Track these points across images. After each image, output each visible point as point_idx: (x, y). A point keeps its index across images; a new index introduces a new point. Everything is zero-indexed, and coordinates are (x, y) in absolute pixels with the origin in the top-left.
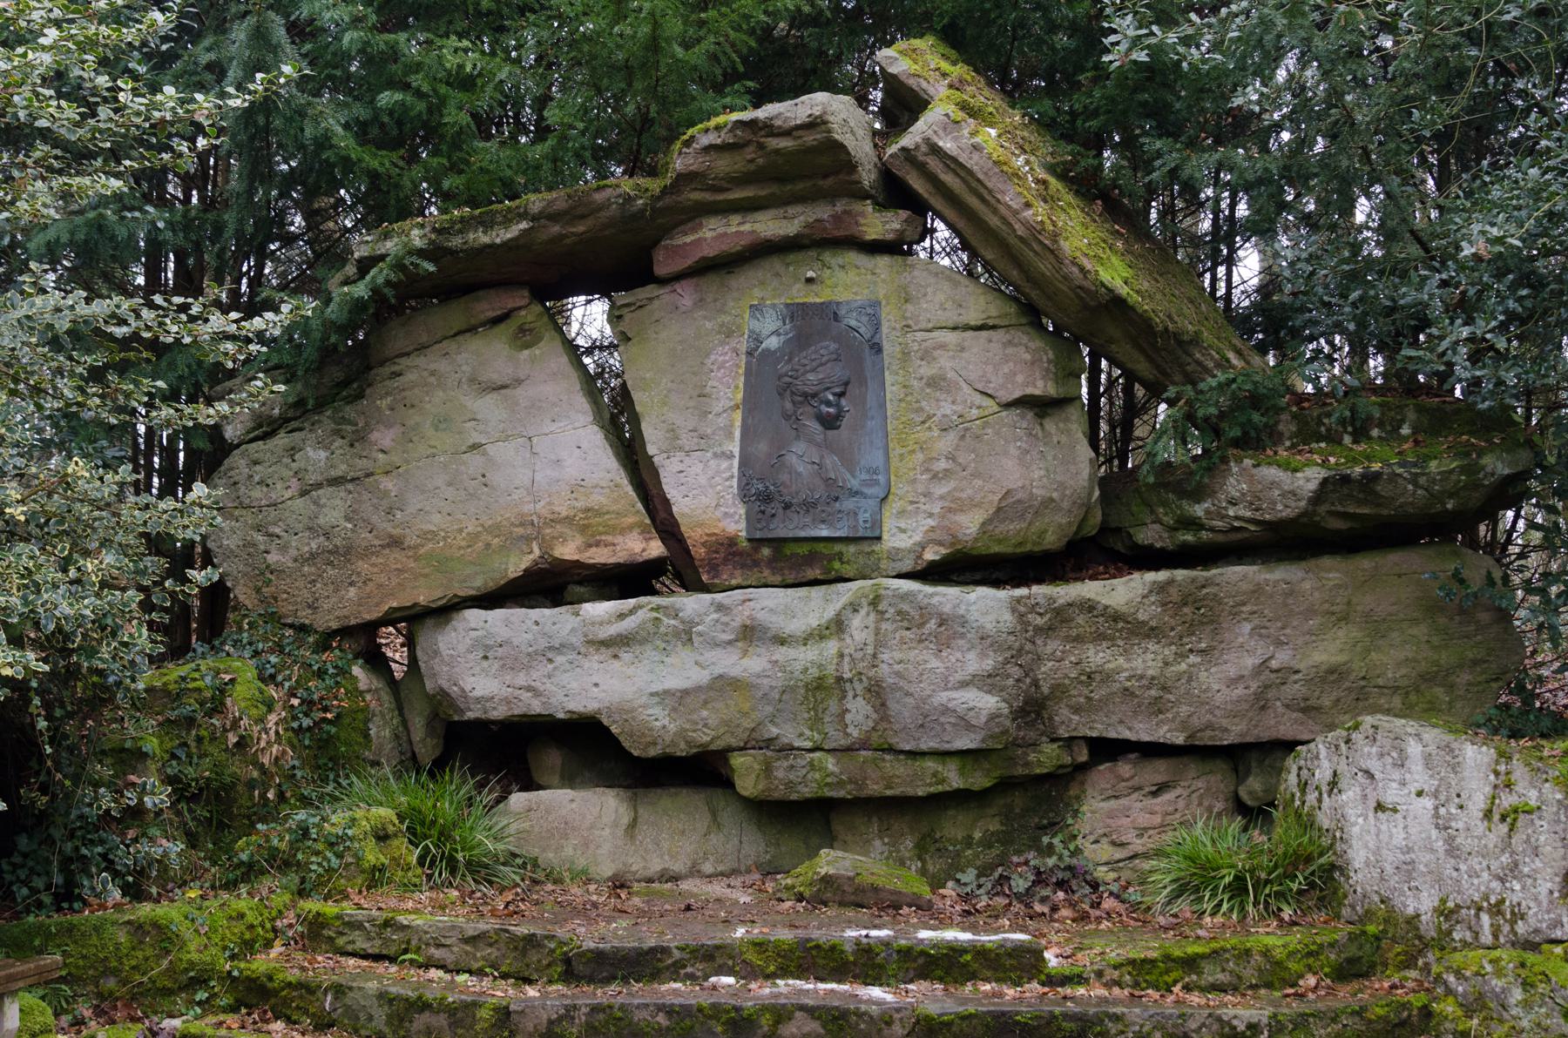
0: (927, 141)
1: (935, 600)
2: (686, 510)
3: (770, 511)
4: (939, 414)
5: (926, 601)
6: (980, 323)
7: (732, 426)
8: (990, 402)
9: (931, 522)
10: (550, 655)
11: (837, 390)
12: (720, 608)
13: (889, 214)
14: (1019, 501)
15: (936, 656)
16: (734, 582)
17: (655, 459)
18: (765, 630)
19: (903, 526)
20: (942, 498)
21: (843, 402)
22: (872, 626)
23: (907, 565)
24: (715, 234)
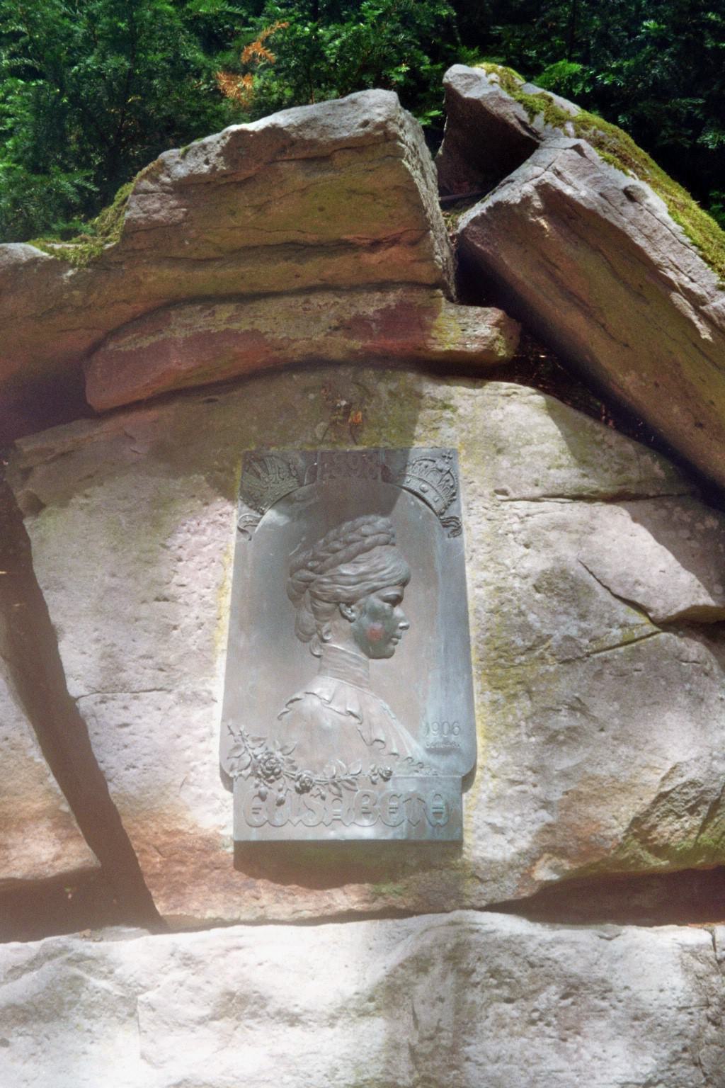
0: (544, 190)
1: (556, 953)
2: (132, 791)
4: (557, 635)
5: (542, 952)
6: (616, 489)
7: (212, 649)
8: (636, 618)
11: (391, 592)
12: (188, 961)
14: (693, 784)
15: (559, 1050)
16: (210, 914)
17: (82, 705)
18: (262, 1001)
19: (498, 821)
20: (565, 775)
21: (398, 612)
22: (450, 997)
23: (509, 889)
24: (178, 347)
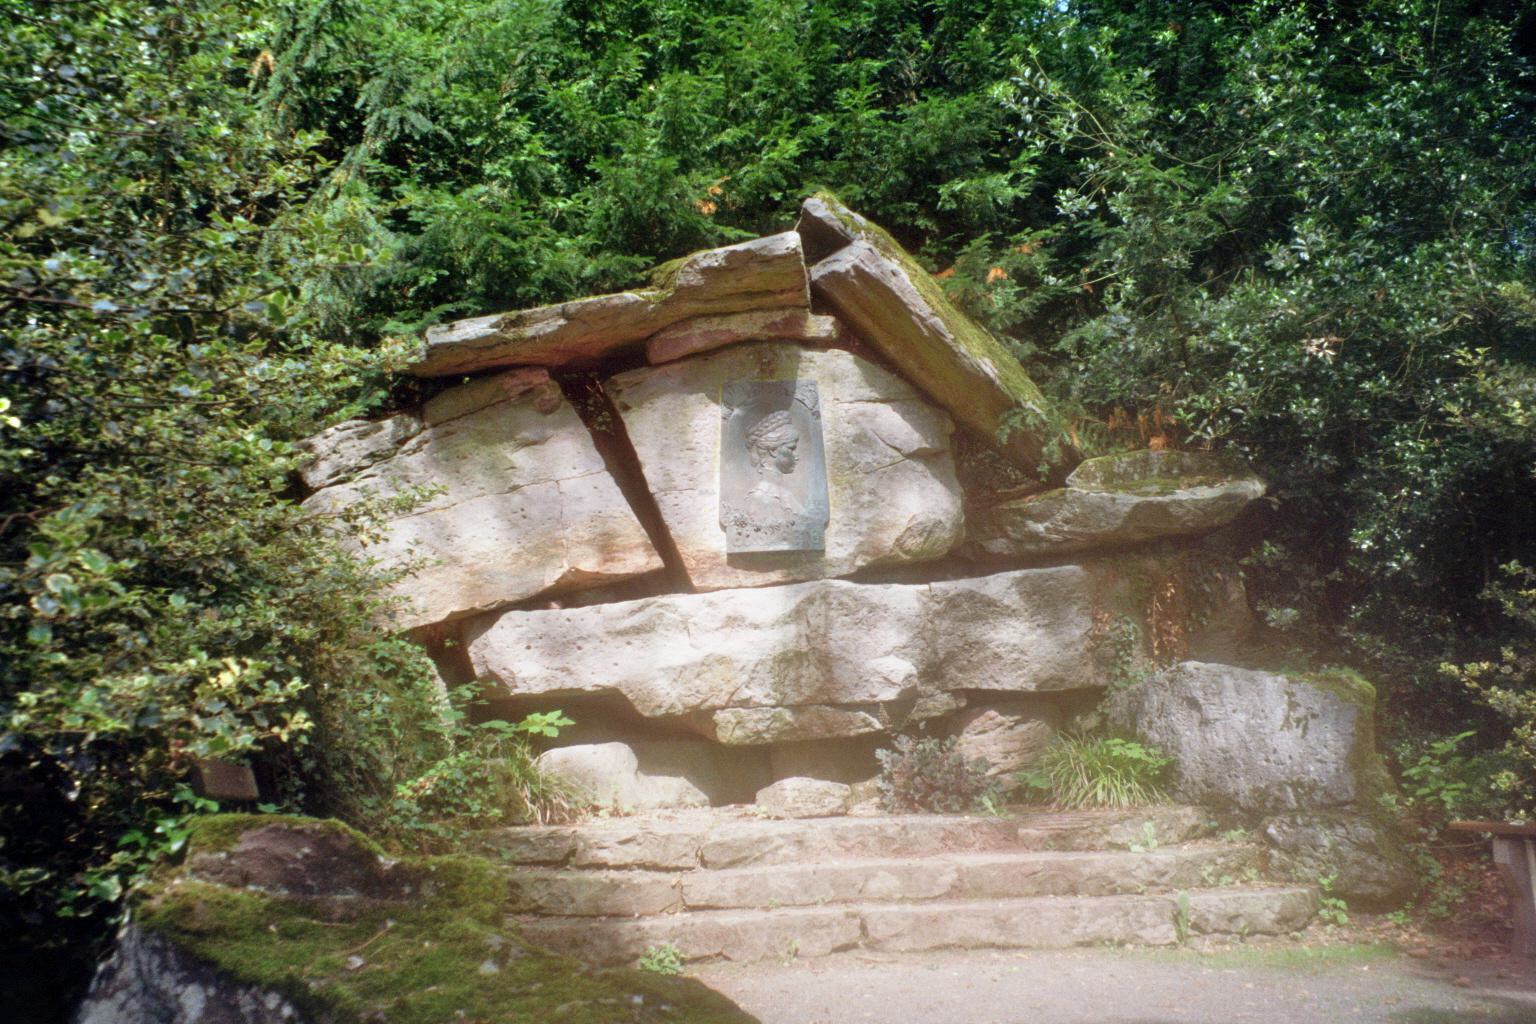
12: (711, 604)
18: (743, 619)
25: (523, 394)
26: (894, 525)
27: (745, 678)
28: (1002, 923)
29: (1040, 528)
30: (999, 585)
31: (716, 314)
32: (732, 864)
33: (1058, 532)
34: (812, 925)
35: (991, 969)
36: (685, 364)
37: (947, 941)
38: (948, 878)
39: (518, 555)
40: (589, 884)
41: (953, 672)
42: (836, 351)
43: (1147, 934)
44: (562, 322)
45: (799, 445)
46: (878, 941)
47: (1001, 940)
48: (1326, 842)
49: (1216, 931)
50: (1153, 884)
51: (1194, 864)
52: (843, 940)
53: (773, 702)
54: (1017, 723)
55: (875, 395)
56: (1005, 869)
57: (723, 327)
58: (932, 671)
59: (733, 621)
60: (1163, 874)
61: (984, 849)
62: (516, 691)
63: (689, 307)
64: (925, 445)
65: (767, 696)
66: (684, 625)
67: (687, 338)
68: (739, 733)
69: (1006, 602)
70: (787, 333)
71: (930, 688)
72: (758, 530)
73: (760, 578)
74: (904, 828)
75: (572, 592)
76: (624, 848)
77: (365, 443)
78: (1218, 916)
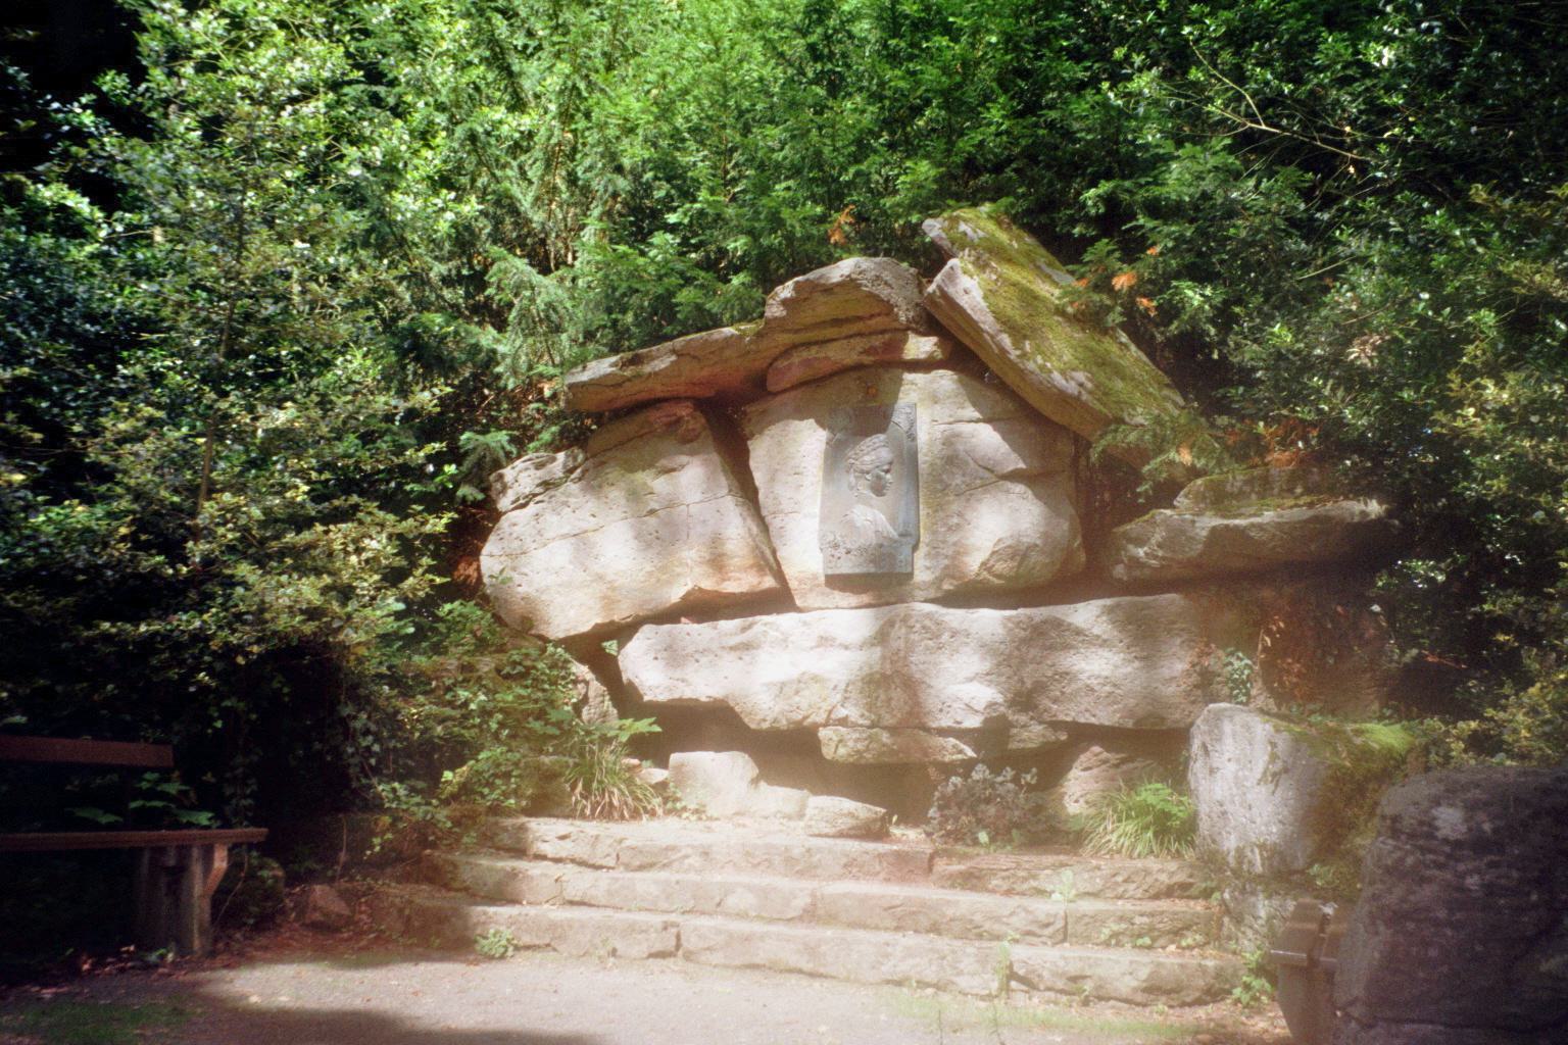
3: (837, 555)
8: (987, 474)
9: (946, 562)
10: (697, 656)
12: (805, 623)
13: (924, 339)
18: (834, 639)
25: (669, 425)
26: (978, 549)
27: (839, 697)
28: (811, 950)
29: (1141, 552)
30: (1086, 614)
31: (816, 343)
32: (641, 868)
33: (1155, 557)
34: (632, 929)
35: (788, 999)
36: (798, 393)
37: (757, 960)
38: (801, 902)
39: (650, 573)
40: (498, 871)
41: (1045, 702)
42: (941, 372)
43: (963, 982)
44: (674, 358)
45: (895, 467)
46: (691, 953)
47: (807, 967)
48: (1263, 913)
49: (1049, 989)
50: (1029, 933)
51: (1097, 920)
52: (658, 947)
53: (867, 722)
54: (1123, 761)
55: (977, 415)
56: (863, 900)
57: (821, 355)
58: (1025, 700)
59: (825, 641)
60: (1047, 925)
61: (887, 880)
62: (646, 698)
63: (785, 339)
64: (1022, 465)
65: (862, 716)
66: (784, 642)
67: (789, 368)
68: (842, 751)
69: (1096, 631)
70: (887, 357)
71: (1023, 718)
72: (848, 552)
73: (853, 600)
74: (809, 850)
75: (703, 608)
76: (562, 842)
77: (539, 473)
78: (1055, 974)
